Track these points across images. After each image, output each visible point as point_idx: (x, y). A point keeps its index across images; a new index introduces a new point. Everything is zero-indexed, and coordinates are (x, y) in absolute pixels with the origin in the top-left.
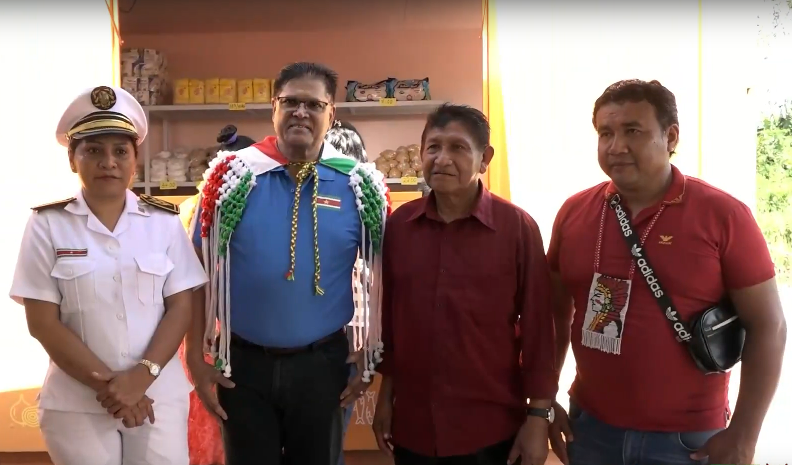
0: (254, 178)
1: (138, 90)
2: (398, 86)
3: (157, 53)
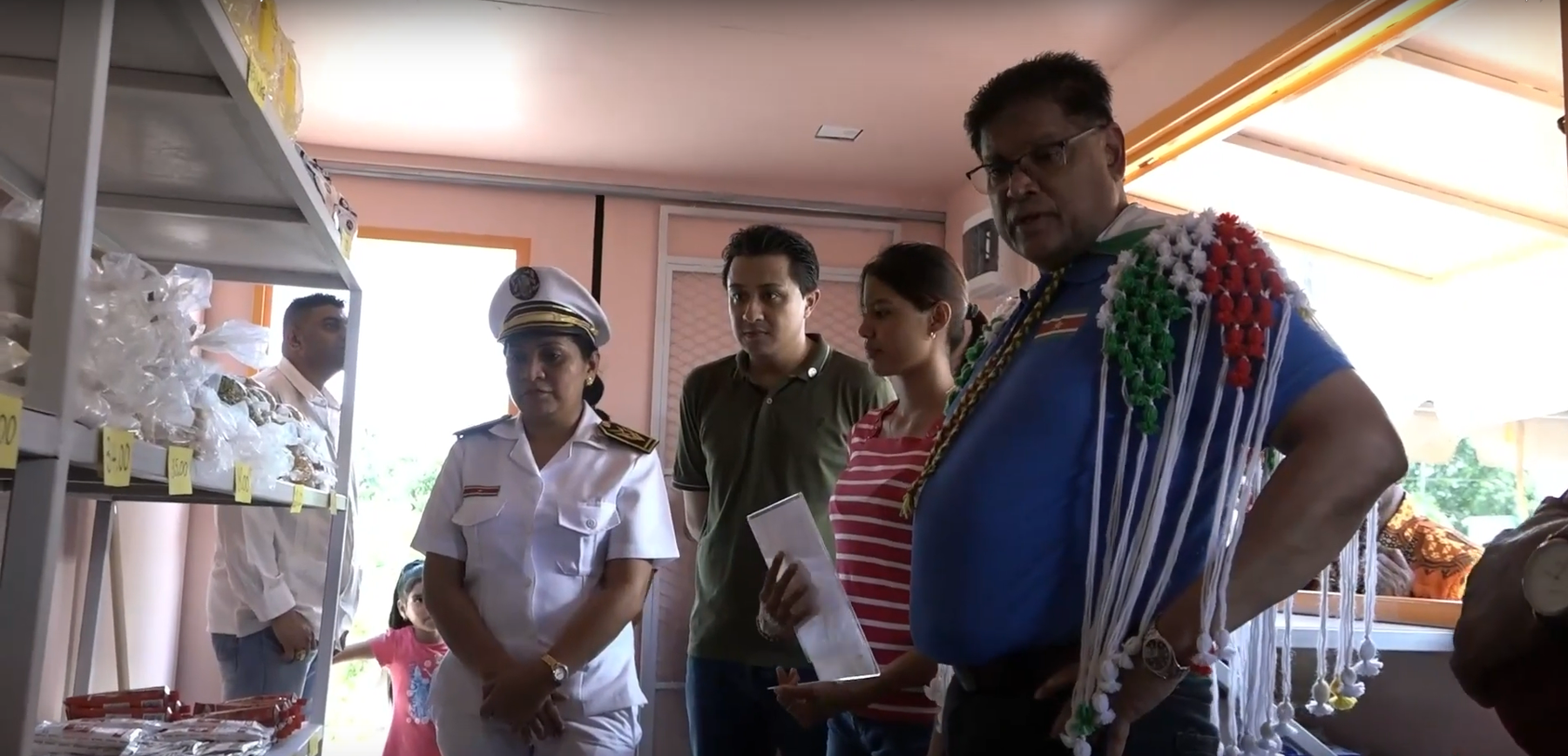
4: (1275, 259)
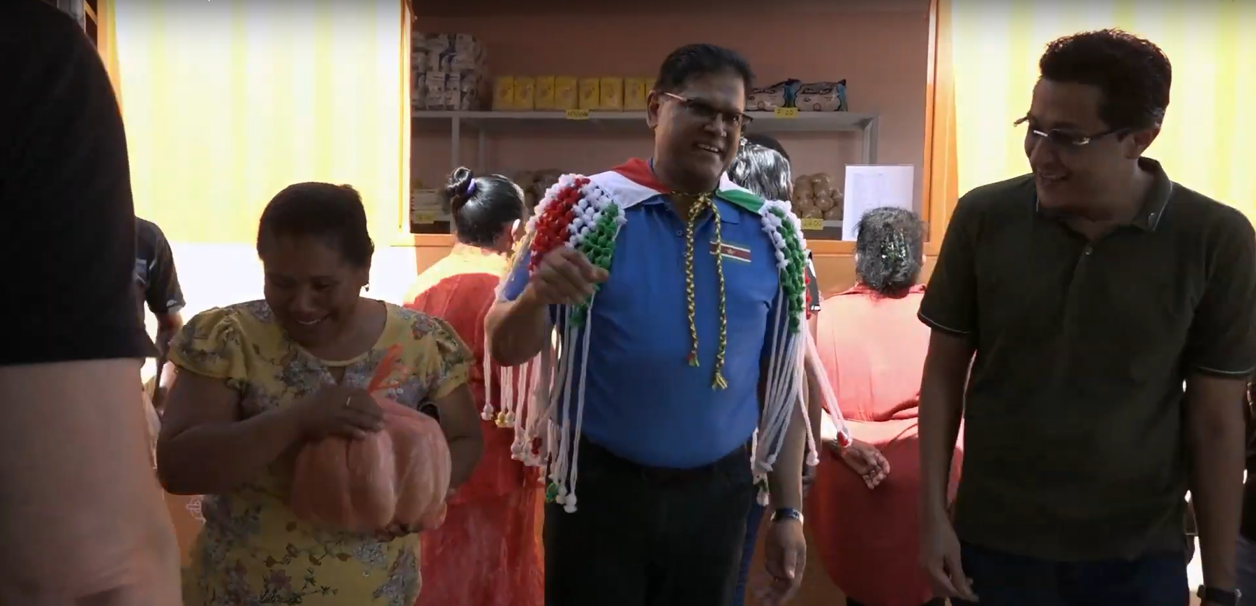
0: (622, 212)
1: (447, 89)
2: (802, 90)
3: (474, 40)
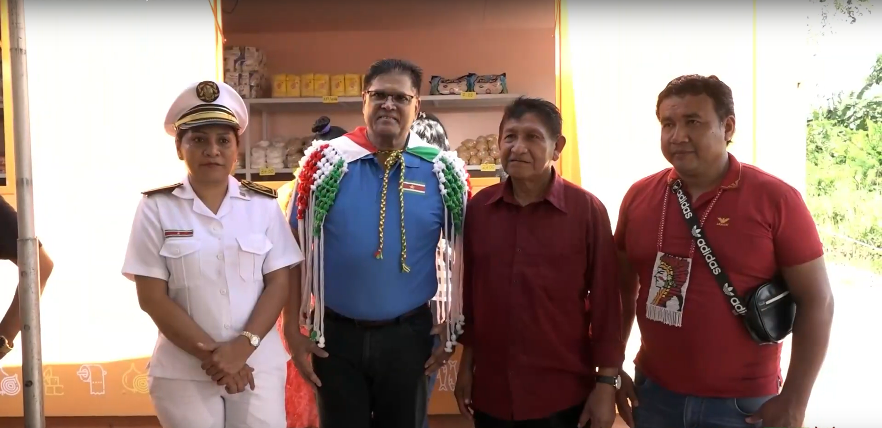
0: (345, 165)
2: (478, 80)
3: (257, 50)
4: (282, 338)
